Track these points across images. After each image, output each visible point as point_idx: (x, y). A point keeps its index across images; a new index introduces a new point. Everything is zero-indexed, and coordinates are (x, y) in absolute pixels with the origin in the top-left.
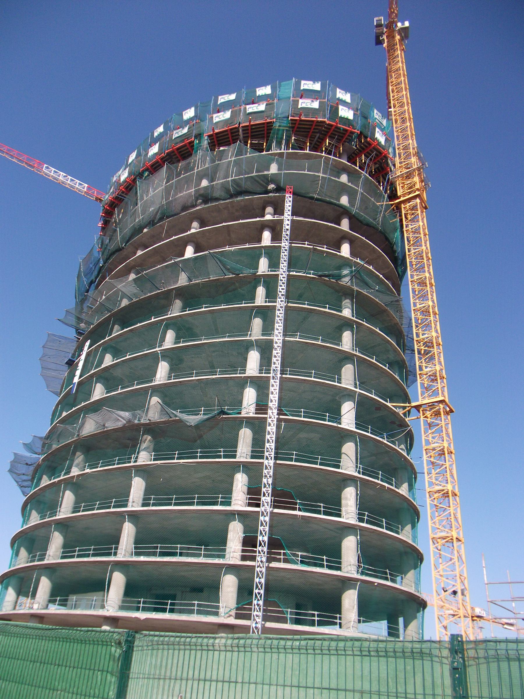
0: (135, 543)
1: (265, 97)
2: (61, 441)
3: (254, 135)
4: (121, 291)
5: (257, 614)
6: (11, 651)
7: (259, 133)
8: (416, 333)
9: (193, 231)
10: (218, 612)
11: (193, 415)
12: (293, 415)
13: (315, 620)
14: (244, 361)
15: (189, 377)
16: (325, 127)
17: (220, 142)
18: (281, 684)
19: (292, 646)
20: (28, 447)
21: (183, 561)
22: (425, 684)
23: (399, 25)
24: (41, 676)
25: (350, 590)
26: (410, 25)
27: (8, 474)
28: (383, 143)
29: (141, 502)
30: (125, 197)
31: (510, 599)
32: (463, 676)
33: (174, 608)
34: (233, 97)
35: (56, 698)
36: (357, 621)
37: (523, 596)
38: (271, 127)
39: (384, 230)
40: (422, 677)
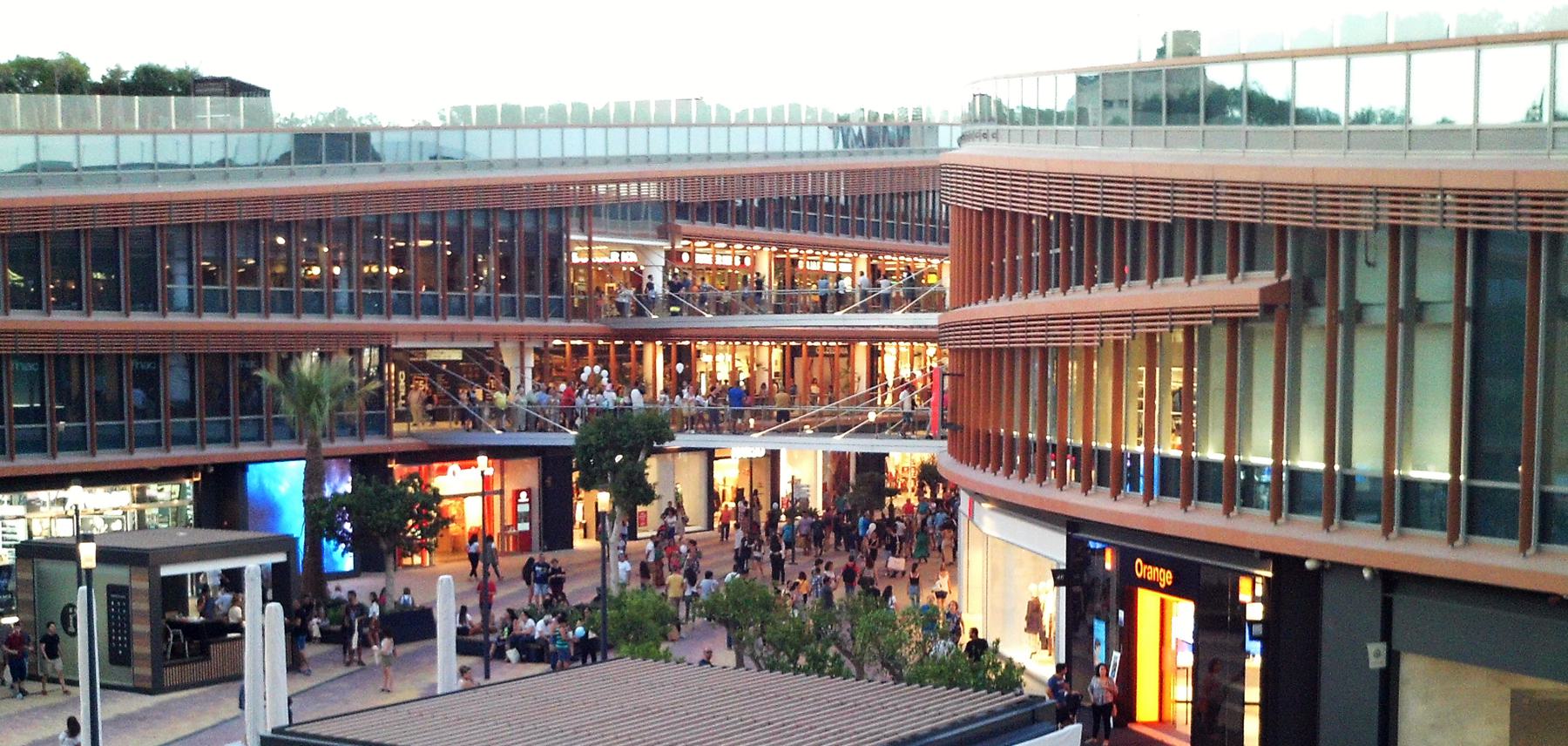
1: (1093, 593)
2: (39, 433)
3: (989, 223)
4: (172, 132)
6: (1475, 213)
8: (1383, 123)
10: (358, 135)
11: (793, 376)
14: (1551, 599)
15: (1532, 405)
17: (1019, 363)
18: (1377, 309)
19: (603, 590)
21: (531, 443)
22: (1541, 28)
26: (1174, 580)
27: (1027, 635)
28: (8, 668)
39: (667, 657)
40: (113, 148)
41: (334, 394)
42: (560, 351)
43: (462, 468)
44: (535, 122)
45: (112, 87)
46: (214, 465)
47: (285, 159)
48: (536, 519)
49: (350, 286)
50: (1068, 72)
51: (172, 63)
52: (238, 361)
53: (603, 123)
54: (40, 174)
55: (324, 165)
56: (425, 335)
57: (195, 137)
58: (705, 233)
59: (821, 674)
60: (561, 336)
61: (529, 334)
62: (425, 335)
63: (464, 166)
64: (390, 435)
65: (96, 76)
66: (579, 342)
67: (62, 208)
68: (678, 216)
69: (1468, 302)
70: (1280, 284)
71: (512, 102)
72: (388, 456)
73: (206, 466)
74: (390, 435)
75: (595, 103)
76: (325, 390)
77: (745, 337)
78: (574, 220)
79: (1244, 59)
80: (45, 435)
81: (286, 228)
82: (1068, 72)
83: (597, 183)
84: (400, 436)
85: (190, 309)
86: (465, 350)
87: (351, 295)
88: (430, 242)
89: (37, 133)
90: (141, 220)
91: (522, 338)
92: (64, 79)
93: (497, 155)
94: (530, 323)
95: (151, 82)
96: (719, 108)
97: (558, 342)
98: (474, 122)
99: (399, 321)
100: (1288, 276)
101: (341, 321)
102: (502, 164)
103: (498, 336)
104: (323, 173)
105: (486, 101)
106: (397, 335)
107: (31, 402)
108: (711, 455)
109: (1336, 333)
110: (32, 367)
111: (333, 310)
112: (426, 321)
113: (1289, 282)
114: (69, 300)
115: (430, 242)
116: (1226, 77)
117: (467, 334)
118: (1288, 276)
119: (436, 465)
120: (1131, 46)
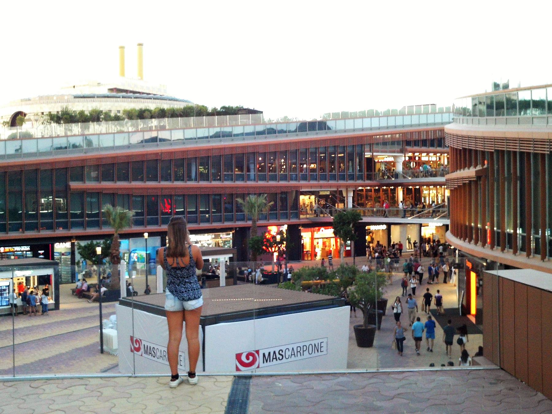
0: (322, 130)
5: (362, 211)
7: (540, 199)
9: (337, 280)
12: (498, 207)
13: (378, 309)
16: (484, 225)
20: (376, 111)
23: (43, 200)
24: (545, 148)
25: (536, 101)
29: (345, 362)
30: (34, 277)
31: (106, 92)
32: (518, 222)
33: (493, 109)
34: (506, 175)
35: (551, 148)
36: (431, 353)
37: (549, 83)
38: (507, 246)
41: (259, 207)
42: (370, 190)
43: (326, 229)
44: (354, 117)
45: (215, 113)
46: (239, 228)
47: (295, 131)
48: (353, 246)
49: (254, 171)
50: (469, 97)
51: (234, 104)
52: (213, 197)
53: (402, 114)
54: (184, 141)
55: (307, 132)
56: (321, 187)
57: (389, 118)
58: (432, 151)
59: (320, 294)
60: (362, 186)
61: (340, 186)
62: (321, 187)
63: (336, 132)
64: (299, 219)
65: (210, 110)
66: (369, 188)
67: (239, 147)
68: (406, 145)
69: (518, 174)
70: (483, 169)
71: (346, 110)
72: (299, 225)
73: (236, 228)
74: (299, 219)
75: (399, 108)
76: (256, 205)
77: (435, 185)
78: (367, 148)
79: (530, 88)
80: (233, 217)
81: (264, 155)
82: (469, 97)
83: (377, 135)
84: (303, 219)
85: (196, 180)
86: (331, 191)
87: (255, 175)
88: (343, 155)
89: (184, 129)
90: (216, 153)
91: (347, 187)
92: (201, 112)
93: (373, 126)
94: (350, 182)
95: (228, 111)
96: (376, 111)
97: (360, 188)
98: (437, 111)
99: (303, 182)
100: (486, 166)
101: (90, 184)
102: (350, 130)
103: (422, 185)
104: (317, 134)
105: (394, 108)
106: (301, 187)
107: (206, 208)
108: (421, 225)
109: (517, 184)
110: (139, 199)
111: (249, 179)
112: (322, 182)
113: (485, 168)
114: (230, 178)
115: (343, 155)
116: (524, 96)
117: (331, 186)
118: (486, 166)
119: (317, 228)
120: (485, 88)
